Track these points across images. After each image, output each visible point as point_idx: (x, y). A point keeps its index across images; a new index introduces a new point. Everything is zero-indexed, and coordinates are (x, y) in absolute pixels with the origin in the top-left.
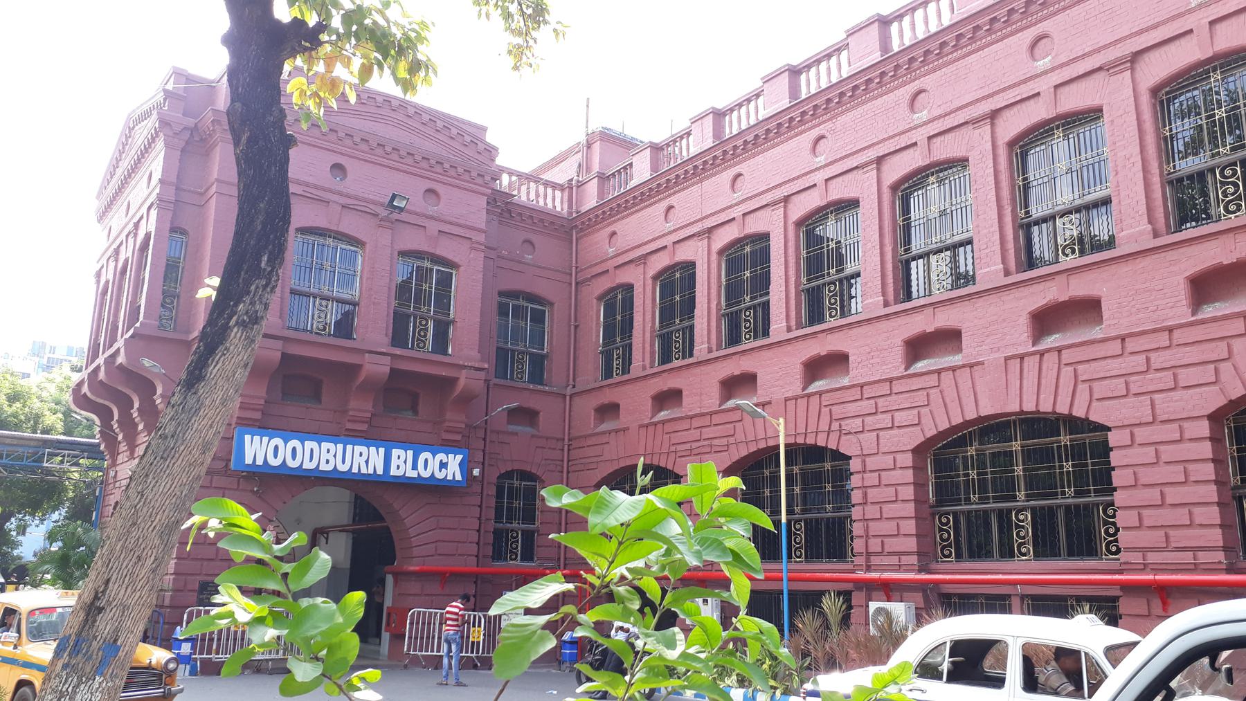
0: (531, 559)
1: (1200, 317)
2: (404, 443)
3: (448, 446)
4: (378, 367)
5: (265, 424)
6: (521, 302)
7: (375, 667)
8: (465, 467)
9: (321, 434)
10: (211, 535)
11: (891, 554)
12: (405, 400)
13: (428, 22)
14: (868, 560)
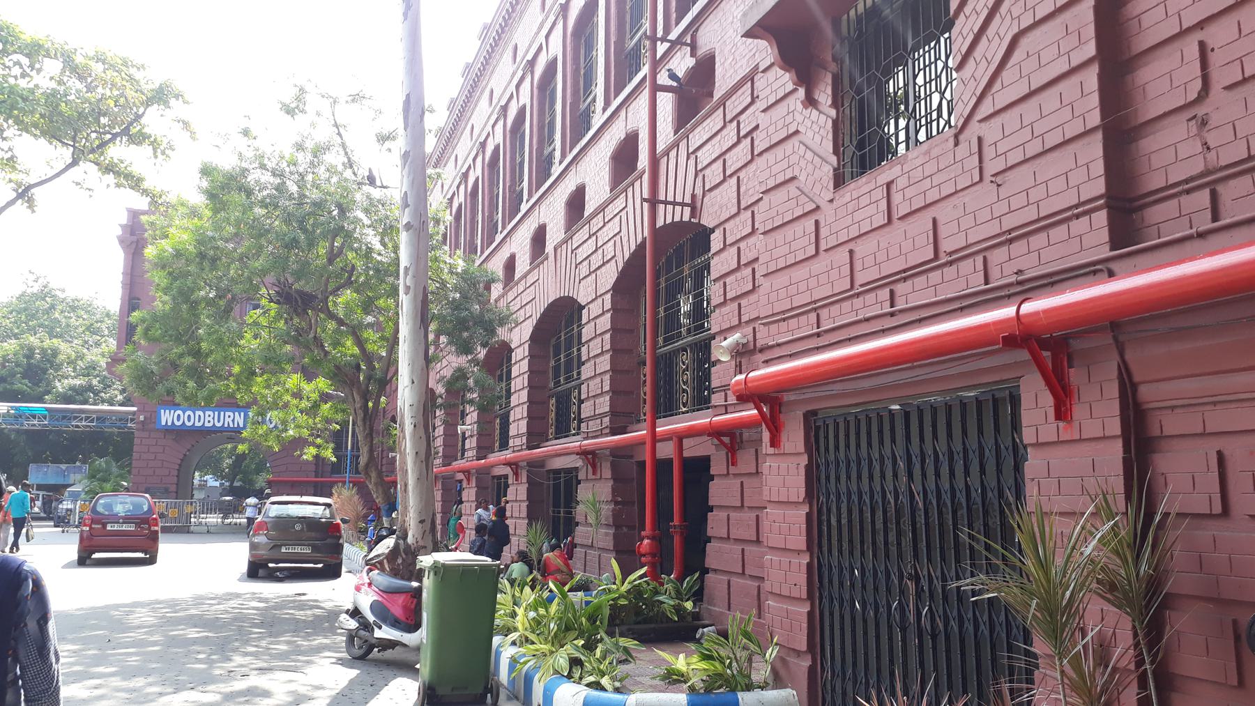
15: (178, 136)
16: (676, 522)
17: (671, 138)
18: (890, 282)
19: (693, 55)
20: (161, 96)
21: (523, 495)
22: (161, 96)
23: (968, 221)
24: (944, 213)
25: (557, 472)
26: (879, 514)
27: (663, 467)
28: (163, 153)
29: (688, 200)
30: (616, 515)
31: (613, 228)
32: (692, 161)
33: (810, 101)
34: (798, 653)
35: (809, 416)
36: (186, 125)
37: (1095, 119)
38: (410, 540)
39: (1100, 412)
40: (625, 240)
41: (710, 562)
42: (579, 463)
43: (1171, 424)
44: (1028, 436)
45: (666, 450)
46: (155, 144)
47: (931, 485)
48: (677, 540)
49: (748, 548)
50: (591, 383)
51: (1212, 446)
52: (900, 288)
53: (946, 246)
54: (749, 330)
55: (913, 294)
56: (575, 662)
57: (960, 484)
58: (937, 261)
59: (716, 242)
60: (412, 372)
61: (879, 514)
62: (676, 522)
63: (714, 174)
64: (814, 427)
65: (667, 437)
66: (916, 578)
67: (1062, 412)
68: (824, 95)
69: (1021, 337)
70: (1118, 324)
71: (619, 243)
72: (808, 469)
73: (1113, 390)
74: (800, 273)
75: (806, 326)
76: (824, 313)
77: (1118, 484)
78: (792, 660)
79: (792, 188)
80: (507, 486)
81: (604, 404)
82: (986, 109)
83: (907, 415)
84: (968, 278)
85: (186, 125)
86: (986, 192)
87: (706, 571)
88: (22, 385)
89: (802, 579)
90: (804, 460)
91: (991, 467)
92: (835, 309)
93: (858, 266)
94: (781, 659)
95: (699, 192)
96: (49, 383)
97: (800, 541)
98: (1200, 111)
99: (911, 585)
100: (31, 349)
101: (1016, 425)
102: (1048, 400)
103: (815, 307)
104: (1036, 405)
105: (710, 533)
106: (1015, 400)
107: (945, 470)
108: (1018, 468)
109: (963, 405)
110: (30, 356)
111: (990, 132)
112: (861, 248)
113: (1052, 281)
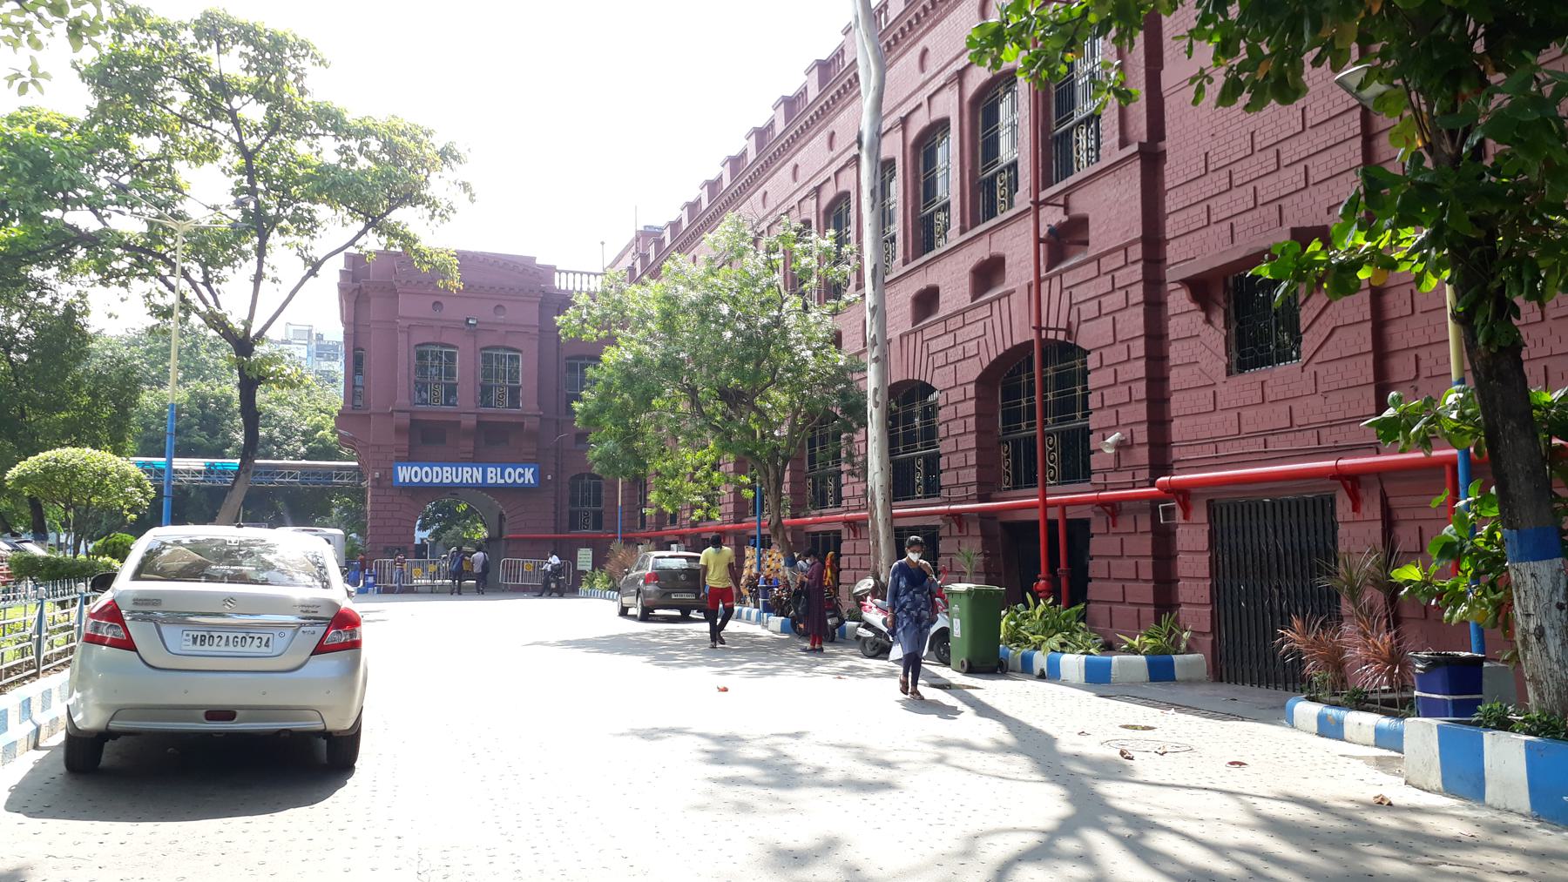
1: (1178, 301)
2: (494, 463)
3: (525, 463)
4: (469, 422)
5: (410, 460)
6: (501, 353)
8: (539, 475)
9: (442, 462)
10: (1548, 91)
12: (490, 440)
14: (831, 474)
15: (460, 199)
16: (1063, 567)
19: (1066, 213)
20: (447, 155)
21: (1202, 541)
22: (447, 155)
23: (1311, 410)
25: (816, 533)
27: (1052, 525)
29: (1063, 325)
30: (986, 564)
31: (977, 329)
32: (1066, 294)
33: (1208, 321)
34: (1204, 634)
35: (1210, 503)
36: (466, 186)
40: (990, 343)
41: (1091, 595)
42: (940, 523)
43: (1401, 515)
44: (1339, 518)
45: (1053, 514)
46: (432, 204)
47: (1288, 541)
49: (1128, 584)
51: (1416, 525)
52: (1270, 439)
54: (1128, 430)
55: (1277, 444)
56: (1063, 645)
62: (1063, 567)
63: (1090, 309)
64: (1212, 507)
65: (1054, 504)
66: (1279, 587)
67: (1355, 508)
68: (1219, 320)
69: (1340, 475)
70: (1380, 474)
72: (1210, 532)
75: (1209, 451)
77: (1379, 540)
79: (1196, 368)
81: (971, 475)
82: (1318, 358)
84: (1308, 440)
85: (466, 186)
86: (1318, 400)
87: (1088, 602)
88: (199, 437)
89: (1207, 593)
90: (1207, 528)
91: (1320, 532)
93: (1243, 422)
94: (1192, 638)
95: (1074, 319)
96: (225, 436)
98: (1415, 384)
99: (1277, 592)
100: (204, 398)
101: (1333, 512)
102: (1349, 503)
103: (1215, 442)
106: (1333, 500)
107: (1296, 533)
108: (1334, 532)
110: (203, 406)
111: (1322, 371)
112: (1245, 413)
113: (1352, 449)
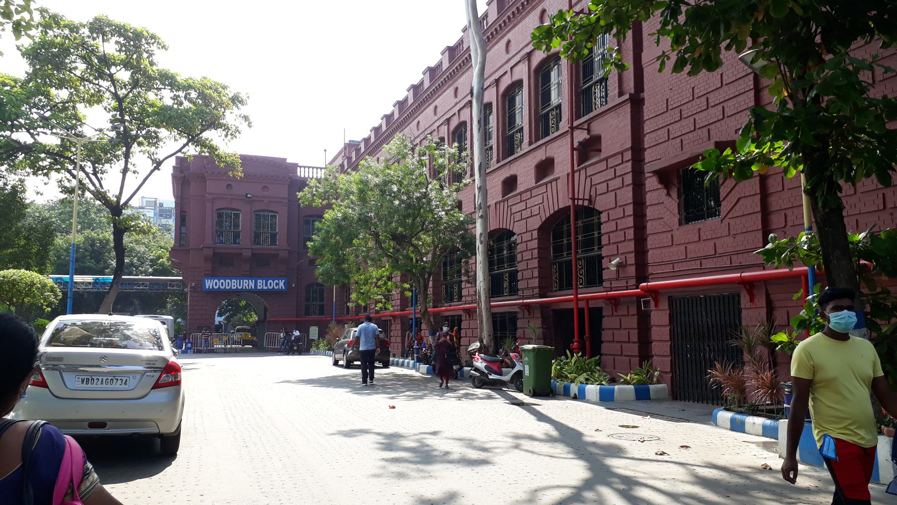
0: (323, 314)
2: (262, 278)
3: (279, 277)
4: (248, 253)
5: (213, 275)
7: (850, 309)
9: (231, 277)
11: (694, 259)
13: (243, 96)
15: (243, 126)
17: (448, 65)
18: (701, 259)
24: (718, 242)
26: (692, 328)
27: (581, 311)
28: (231, 135)
29: (587, 197)
30: (544, 334)
31: (539, 199)
33: (668, 194)
34: (666, 373)
35: (670, 298)
36: (246, 118)
37: (752, 87)
38: (485, 342)
39: (761, 301)
40: (546, 207)
42: (518, 310)
44: (743, 306)
45: (582, 304)
48: (587, 343)
50: (525, 273)
52: (703, 261)
53: (719, 251)
54: (623, 257)
55: (708, 264)
57: (723, 319)
58: (715, 255)
59: (604, 217)
60: (484, 275)
61: (692, 328)
63: (602, 188)
64: (670, 299)
65: (582, 299)
66: (709, 346)
67: (752, 300)
68: (674, 194)
69: (743, 282)
71: (542, 208)
73: (764, 296)
74: (665, 251)
75: (669, 269)
76: (676, 265)
77: (765, 318)
78: (664, 375)
80: (461, 321)
81: (535, 283)
82: (730, 215)
83: (705, 299)
85: (246, 118)
87: (601, 355)
88: (91, 263)
89: (668, 349)
92: (680, 264)
93: (688, 252)
95: (593, 194)
96: (105, 262)
97: (668, 338)
98: (785, 230)
99: (707, 348)
100: (93, 240)
102: (748, 297)
103: (673, 263)
104: (745, 300)
105: (603, 339)
106: (739, 296)
109: (724, 296)
110: (93, 245)
111: (732, 222)
112: (689, 247)
